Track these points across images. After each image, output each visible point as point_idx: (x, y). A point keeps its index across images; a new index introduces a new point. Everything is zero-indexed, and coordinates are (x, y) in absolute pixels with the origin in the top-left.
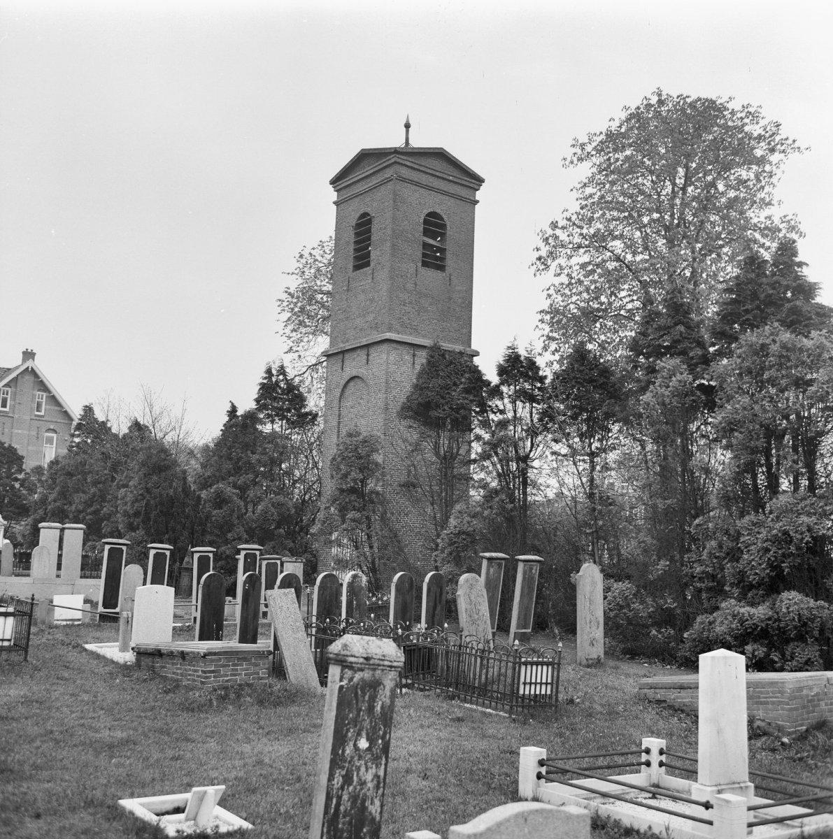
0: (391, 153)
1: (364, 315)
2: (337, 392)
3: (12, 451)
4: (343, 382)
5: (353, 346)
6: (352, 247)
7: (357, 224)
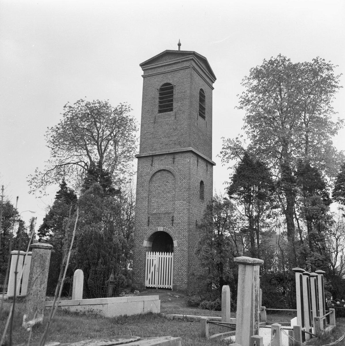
0: (192, 54)
1: (169, 137)
2: (148, 178)
3: (9, 206)
4: (152, 173)
5: (161, 153)
6: (157, 101)
7: (160, 89)
